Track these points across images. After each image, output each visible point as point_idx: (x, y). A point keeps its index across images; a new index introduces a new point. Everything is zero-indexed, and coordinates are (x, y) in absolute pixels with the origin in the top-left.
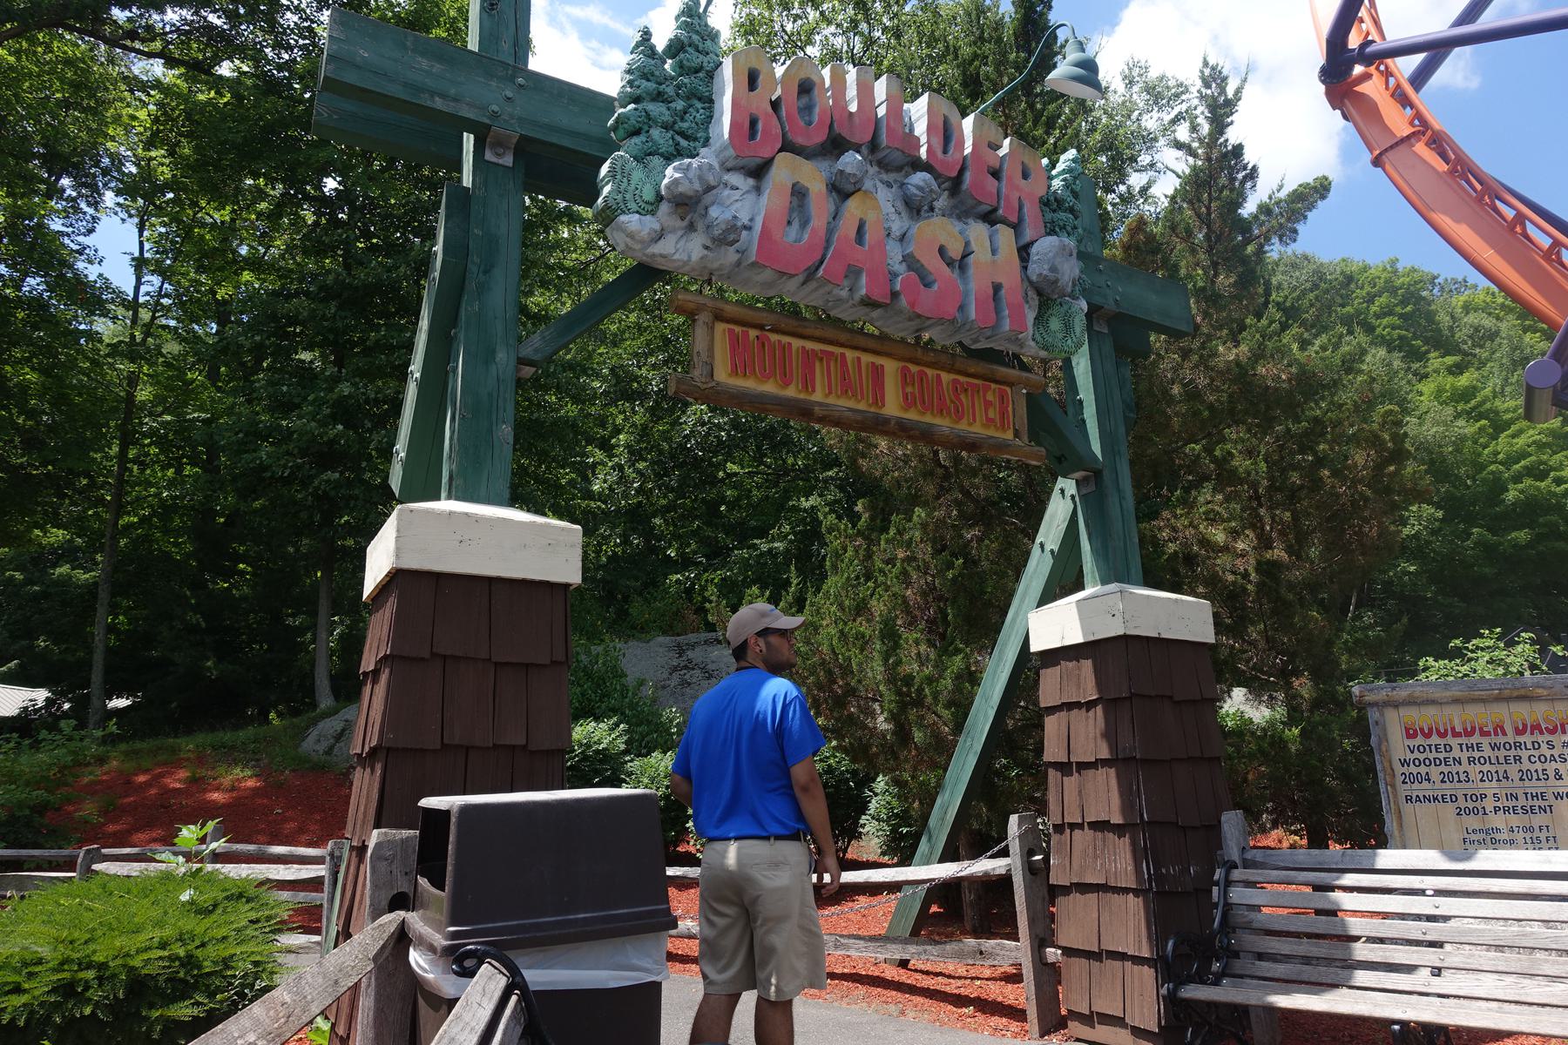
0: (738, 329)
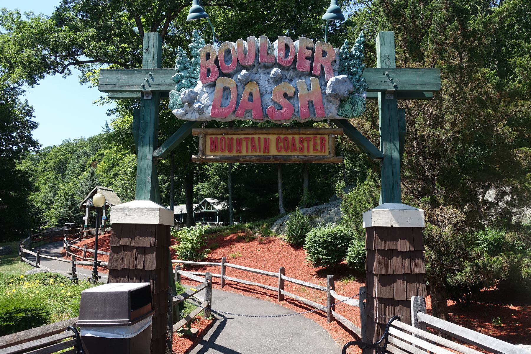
0: (213, 137)
